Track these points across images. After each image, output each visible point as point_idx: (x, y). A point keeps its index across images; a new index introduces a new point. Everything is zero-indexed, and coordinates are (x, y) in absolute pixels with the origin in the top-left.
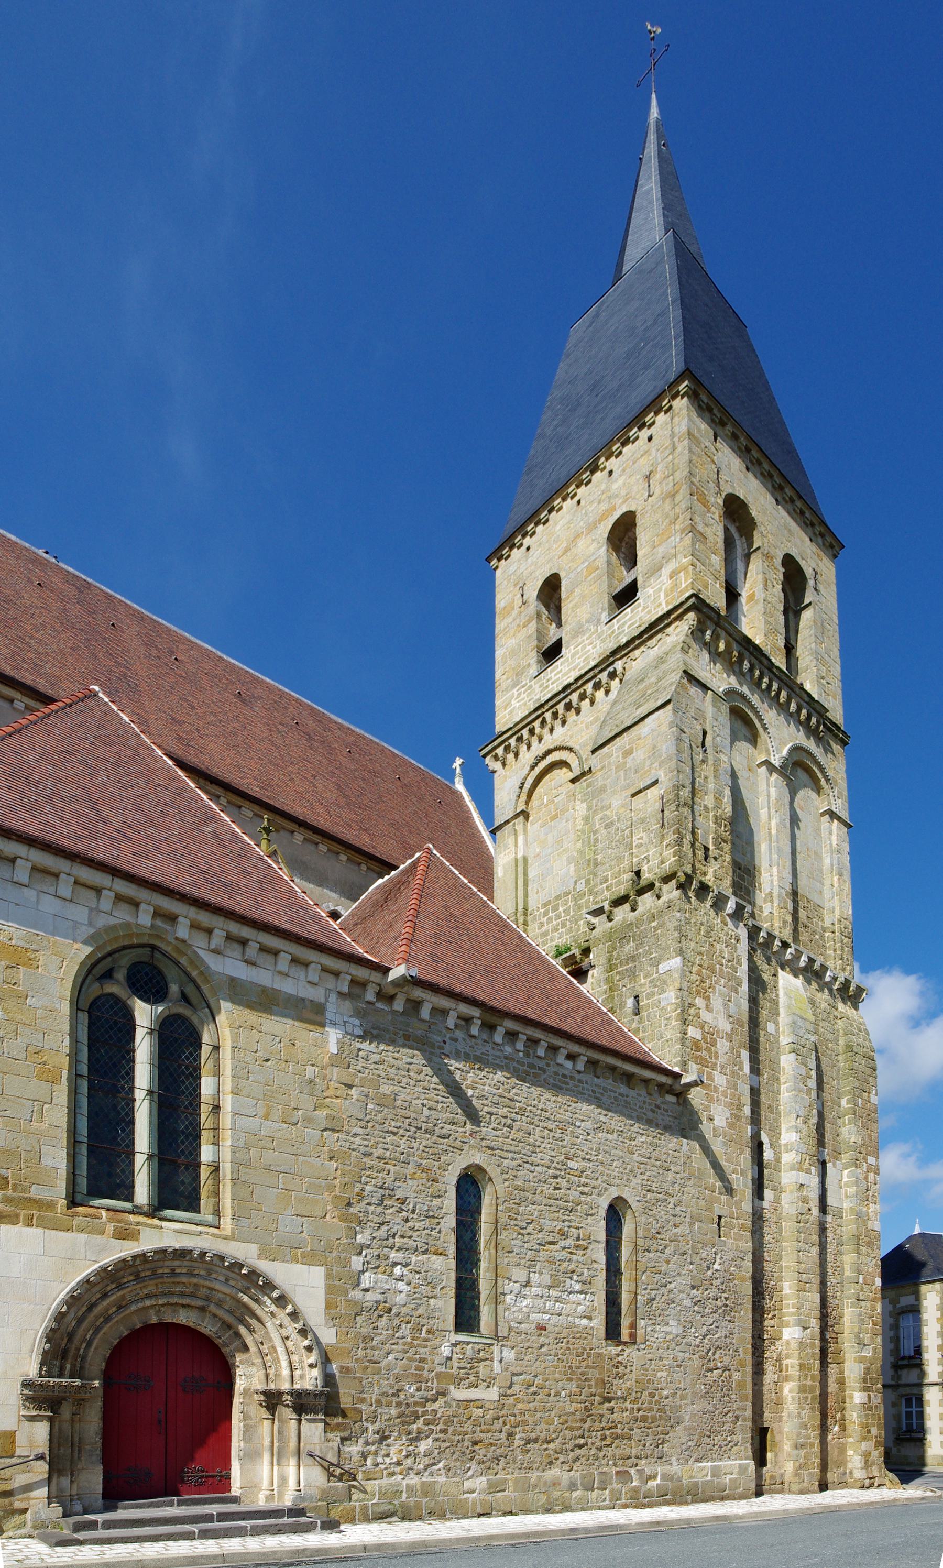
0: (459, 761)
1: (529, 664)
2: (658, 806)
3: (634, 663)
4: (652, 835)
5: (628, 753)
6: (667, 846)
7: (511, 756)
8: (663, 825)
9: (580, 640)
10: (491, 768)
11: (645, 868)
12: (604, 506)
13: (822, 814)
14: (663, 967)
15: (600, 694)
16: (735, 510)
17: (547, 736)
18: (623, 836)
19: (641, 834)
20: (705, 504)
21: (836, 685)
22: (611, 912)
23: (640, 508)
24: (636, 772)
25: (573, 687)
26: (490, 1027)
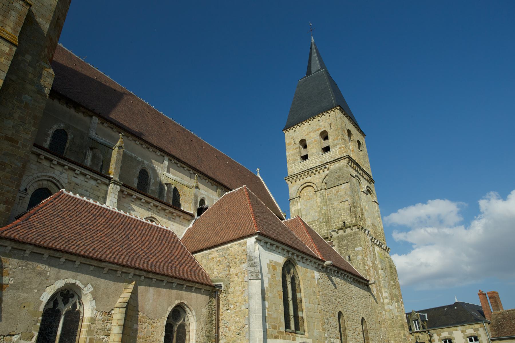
0: (258, 169)
2: (348, 206)
7: (294, 181)
12: (317, 128)
14: (357, 249)
15: (321, 171)
16: (349, 132)
17: (305, 178)
20: (345, 132)
21: (370, 169)
26: (338, 272)
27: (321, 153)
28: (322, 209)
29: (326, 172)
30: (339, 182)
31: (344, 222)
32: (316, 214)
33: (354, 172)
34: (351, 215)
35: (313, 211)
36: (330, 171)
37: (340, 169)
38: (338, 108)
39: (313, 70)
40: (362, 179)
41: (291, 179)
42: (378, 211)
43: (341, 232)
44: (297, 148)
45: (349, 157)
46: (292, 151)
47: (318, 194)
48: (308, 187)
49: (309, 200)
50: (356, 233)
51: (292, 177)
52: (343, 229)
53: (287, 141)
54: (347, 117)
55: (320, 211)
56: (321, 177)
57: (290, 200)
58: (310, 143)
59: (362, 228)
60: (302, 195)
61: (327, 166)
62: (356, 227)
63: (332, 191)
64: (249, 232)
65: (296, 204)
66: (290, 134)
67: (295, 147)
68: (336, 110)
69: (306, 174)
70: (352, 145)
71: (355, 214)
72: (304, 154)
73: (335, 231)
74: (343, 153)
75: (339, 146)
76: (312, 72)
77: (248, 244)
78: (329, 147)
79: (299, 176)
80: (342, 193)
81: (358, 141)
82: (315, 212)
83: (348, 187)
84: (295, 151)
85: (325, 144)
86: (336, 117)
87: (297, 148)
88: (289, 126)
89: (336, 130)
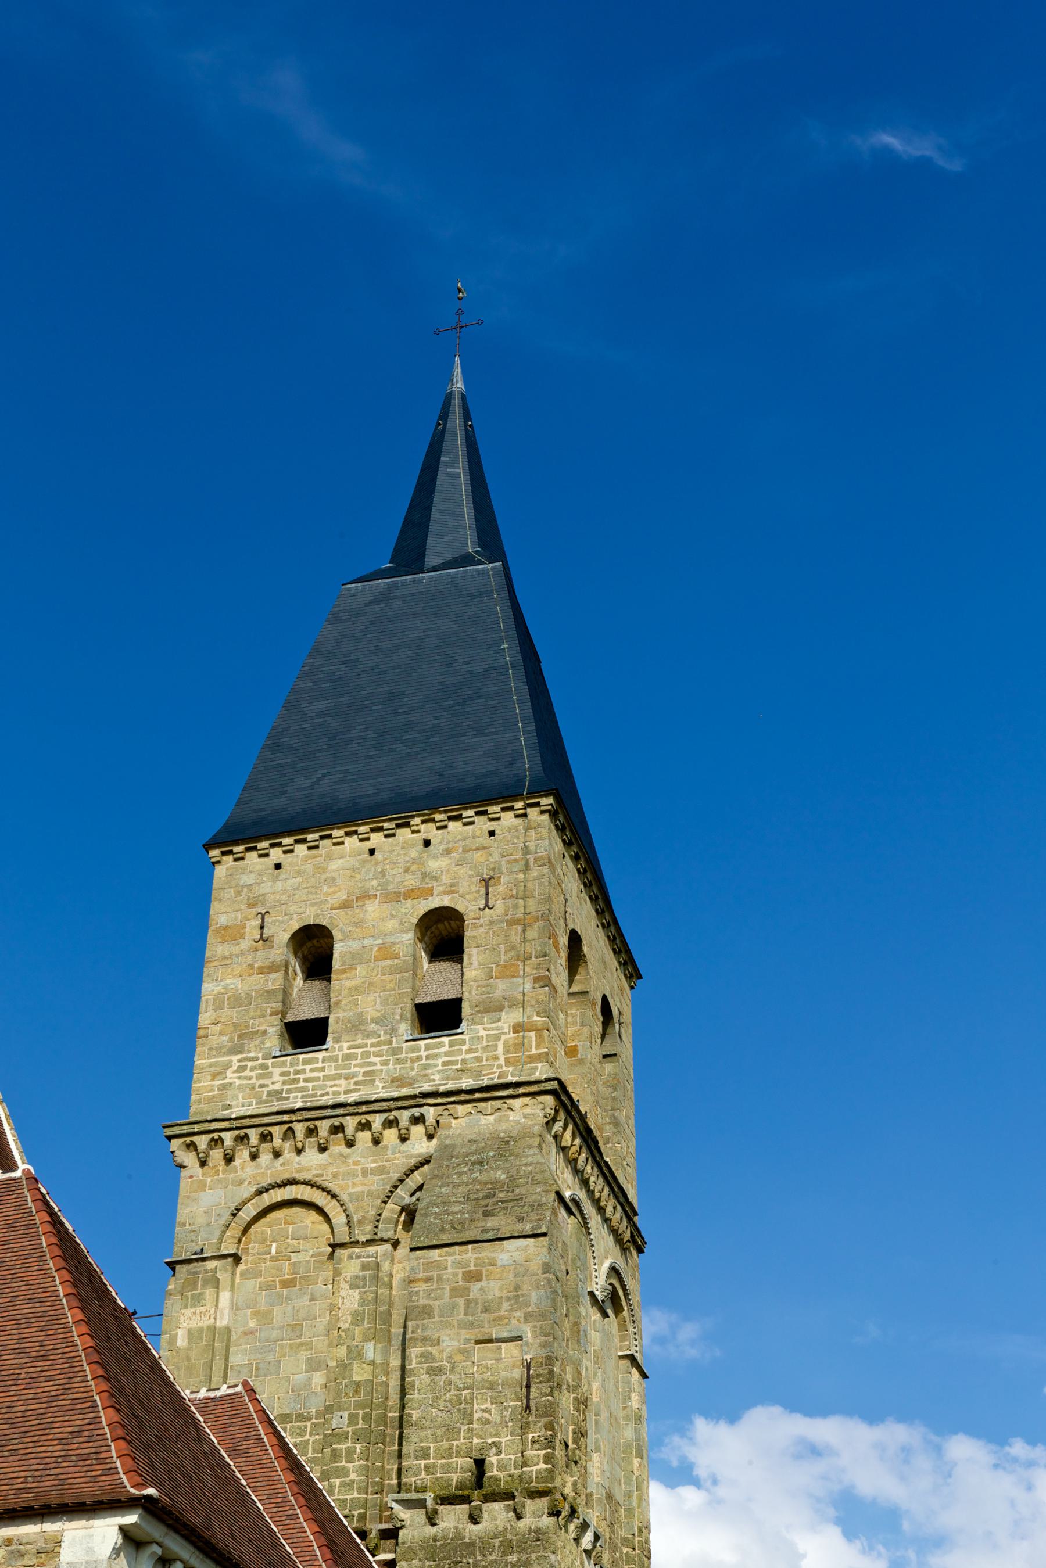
1: (265, 1032)
2: (518, 1373)
3: (454, 1121)
4: (507, 1414)
5: (473, 1276)
6: (534, 1442)
8: (528, 1406)
9: (360, 1041)
10: (179, 1160)
11: (492, 1459)
12: (412, 881)
13: (622, 1357)
15: (390, 1136)
16: (575, 939)
17: (288, 1155)
18: (459, 1397)
19: (488, 1405)
20: (556, 945)
22: (436, 1512)
23: (472, 915)
24: (486, 1310)
25: (351, 1110)
27: (405, 1029)
28: (356, 1354)
29: (420, 1145)
30: (491, 1223)
31: (480, 1464)
32: (318, 1378)
33: (568, 1176)
34: (524, 1428)
35: (304, 1355)
36: (443, 1148)
37: (505, 1146)
38: (547, 801)
39: (436, 551)
40: (595, 1220)
41: (202, 1142)
42: (638, 1419)
43: (452, 1518)
44: (272, 968)
45: (561, 1093)
46: (238, 979)
47: (351, 1264)
48: (296, 1210)
49: (288, 1284)
50: (538, 1536)
51: (214, 1128)
52: (466, 1500)
53: (223, 913)
54: (576, 858)
55: (344, 1367)
56: (381, 1170)
57: (172, 1265)
58: (356, 959)
59: (573, 1512)
60: (254, 1247)
61: (430, 1113)
62: (543, 1503)
63: (441, 1267)
64: (80, 1485)
65: (209, 1293)
66: (246, 879)
67: (261, 959)
68: (532, 812)
69: (300, 1129)
70: (579, 1023)
71: (550, 1426)
72: (305, 1011)
73: (421, 1504)
74: (533, 1059)
75: (515, 1016)
76: (431, 560)
77: (66, 1554)
78: (455, 1005)
79: (254, 1135)
80: (493, 1288)
81: (605, 998)
82: (313, 1365)
83: (535, 1266)
84: (256, 982)
85: (438, 982)
86: (526, 850)
87: (272, 968)
88: (248, 830)
89: (514, 922)
